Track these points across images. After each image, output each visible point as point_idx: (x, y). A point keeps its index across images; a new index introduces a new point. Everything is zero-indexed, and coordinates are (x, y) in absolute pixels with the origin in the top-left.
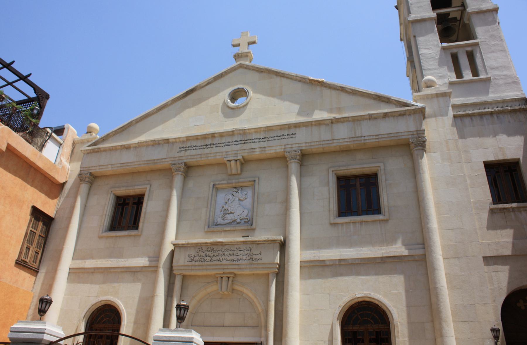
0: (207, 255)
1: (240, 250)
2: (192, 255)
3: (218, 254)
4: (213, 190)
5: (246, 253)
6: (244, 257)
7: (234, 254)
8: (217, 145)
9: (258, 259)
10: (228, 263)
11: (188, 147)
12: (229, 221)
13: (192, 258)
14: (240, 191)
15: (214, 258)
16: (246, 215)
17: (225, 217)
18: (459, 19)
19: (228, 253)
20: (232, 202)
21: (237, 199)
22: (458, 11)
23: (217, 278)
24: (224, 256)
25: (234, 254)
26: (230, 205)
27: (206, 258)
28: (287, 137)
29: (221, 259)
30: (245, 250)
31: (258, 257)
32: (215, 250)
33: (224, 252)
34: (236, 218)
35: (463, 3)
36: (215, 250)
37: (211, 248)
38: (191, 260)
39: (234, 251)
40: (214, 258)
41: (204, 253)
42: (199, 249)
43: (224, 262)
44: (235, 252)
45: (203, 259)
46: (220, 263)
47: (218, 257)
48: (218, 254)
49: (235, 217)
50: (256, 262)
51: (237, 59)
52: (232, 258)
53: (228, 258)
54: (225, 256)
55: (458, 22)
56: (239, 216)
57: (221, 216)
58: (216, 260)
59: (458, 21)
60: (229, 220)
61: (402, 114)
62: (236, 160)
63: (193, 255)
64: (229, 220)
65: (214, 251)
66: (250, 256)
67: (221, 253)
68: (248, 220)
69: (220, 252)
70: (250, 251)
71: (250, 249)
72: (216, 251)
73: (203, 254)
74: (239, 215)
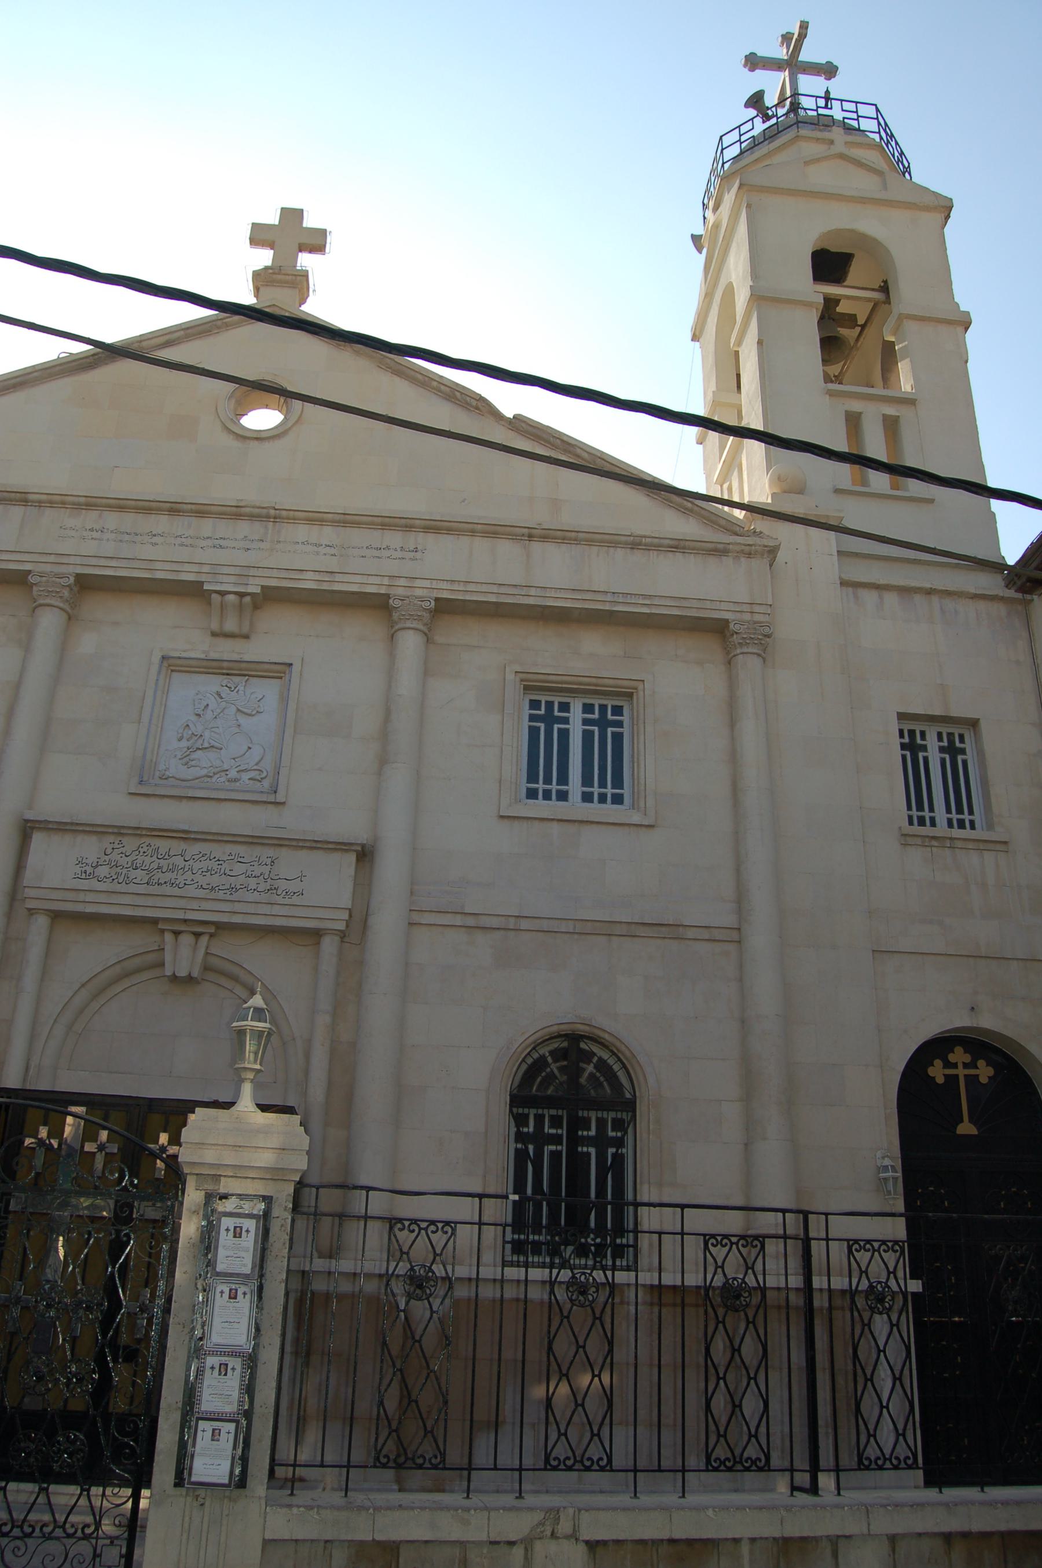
0: (138, 865)
1: (239, 860)
2: (89, 861)
3: (171, 867)
4: (159, 673)
5: (257, 873)
6: (252, 883)
7: (222, 871)
8: (183, 540)
9: (294, 893)
10: (201, 893)
11: (91, 530)
12: (204, 772)
13: (89, 870)
14: (242, 688)
15: (158, 876)
16: (257, 759)
17: (193, 756)
18: (861, 321)
19: (205, 864)
20: (216, 718)
21: (233, 709)
22: (869, 300)
23: (163, 931)
24: (190, 872)
25: (222, 871)
26: (210, 726)
27: (133, 874)
28: (399, 554)
29: (181, 880)
30: (256, 864)
31: (293, 887)
32: (162, 851)
33: (191, 862)
34: (226, 767)
35: (885, 282)
36: (162, 851)
37: (149, 845)
38: (84, 874)
39: (220, 862)
40: (158, 876)
41: (129, 859)
42: (112, 846)
43: (192, 891)
44: (224, 865)
45: (123, 876)
46: (176, 891)
47: (173, 876)
48: (171, 867)
49: (223, 762)
50: (287, 901)
51: (262, 289)
52: (215, 880)
53: (203, 881)
54: (193, 874)
55: (858, 329)
56: (234, 759)
57: (179, 754)
58: (165, 883)
59: (859, 326)
60: (202, 768)
61: (719, 551)
62: (242, 595)
63: (92, 859)
64: (202, 768)
65: (160, 857)
66: (269, 880)
67: (182, 864)
68: (263, 775)
69: (179, 861)
70: (269, 866)
71: (269, 861)
72: (167, 857)
73: (124, 861)
74: (234, 757)
